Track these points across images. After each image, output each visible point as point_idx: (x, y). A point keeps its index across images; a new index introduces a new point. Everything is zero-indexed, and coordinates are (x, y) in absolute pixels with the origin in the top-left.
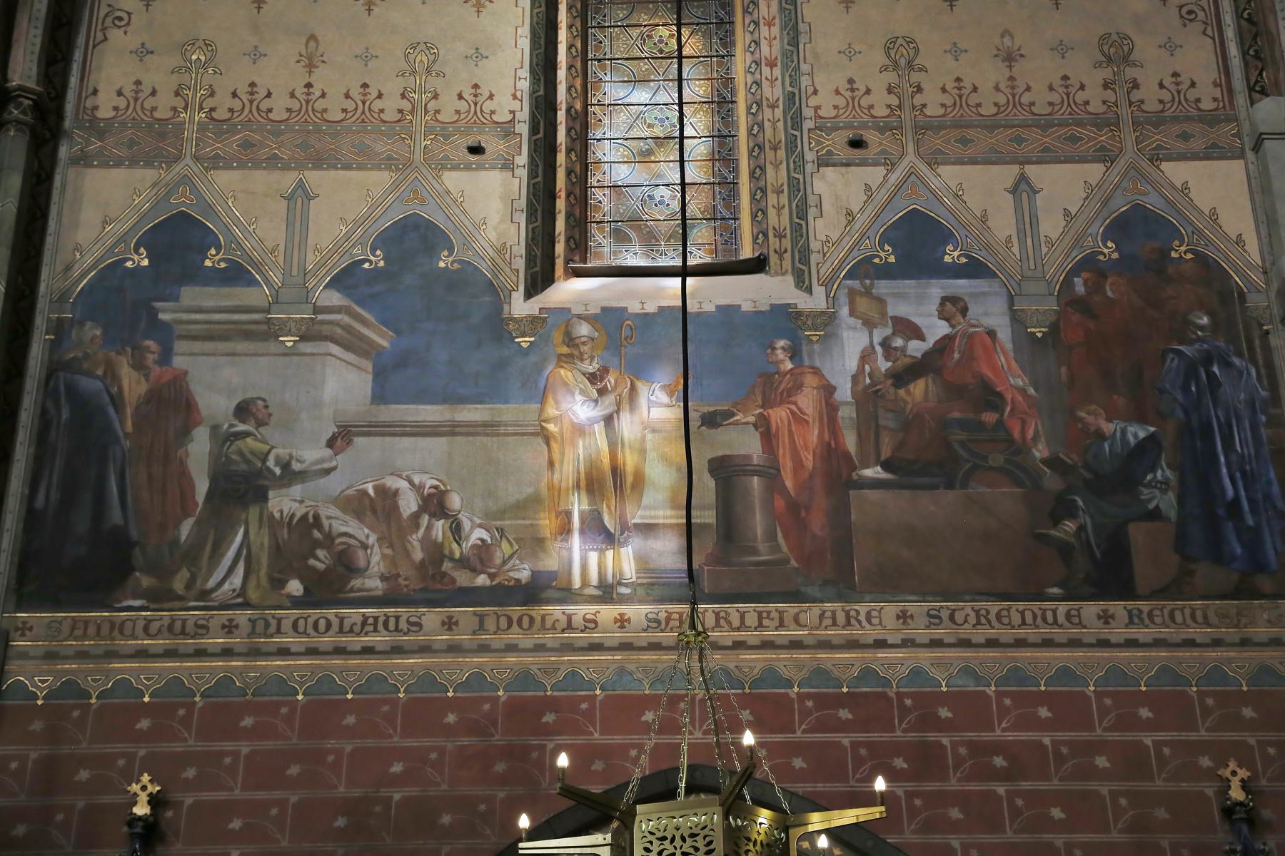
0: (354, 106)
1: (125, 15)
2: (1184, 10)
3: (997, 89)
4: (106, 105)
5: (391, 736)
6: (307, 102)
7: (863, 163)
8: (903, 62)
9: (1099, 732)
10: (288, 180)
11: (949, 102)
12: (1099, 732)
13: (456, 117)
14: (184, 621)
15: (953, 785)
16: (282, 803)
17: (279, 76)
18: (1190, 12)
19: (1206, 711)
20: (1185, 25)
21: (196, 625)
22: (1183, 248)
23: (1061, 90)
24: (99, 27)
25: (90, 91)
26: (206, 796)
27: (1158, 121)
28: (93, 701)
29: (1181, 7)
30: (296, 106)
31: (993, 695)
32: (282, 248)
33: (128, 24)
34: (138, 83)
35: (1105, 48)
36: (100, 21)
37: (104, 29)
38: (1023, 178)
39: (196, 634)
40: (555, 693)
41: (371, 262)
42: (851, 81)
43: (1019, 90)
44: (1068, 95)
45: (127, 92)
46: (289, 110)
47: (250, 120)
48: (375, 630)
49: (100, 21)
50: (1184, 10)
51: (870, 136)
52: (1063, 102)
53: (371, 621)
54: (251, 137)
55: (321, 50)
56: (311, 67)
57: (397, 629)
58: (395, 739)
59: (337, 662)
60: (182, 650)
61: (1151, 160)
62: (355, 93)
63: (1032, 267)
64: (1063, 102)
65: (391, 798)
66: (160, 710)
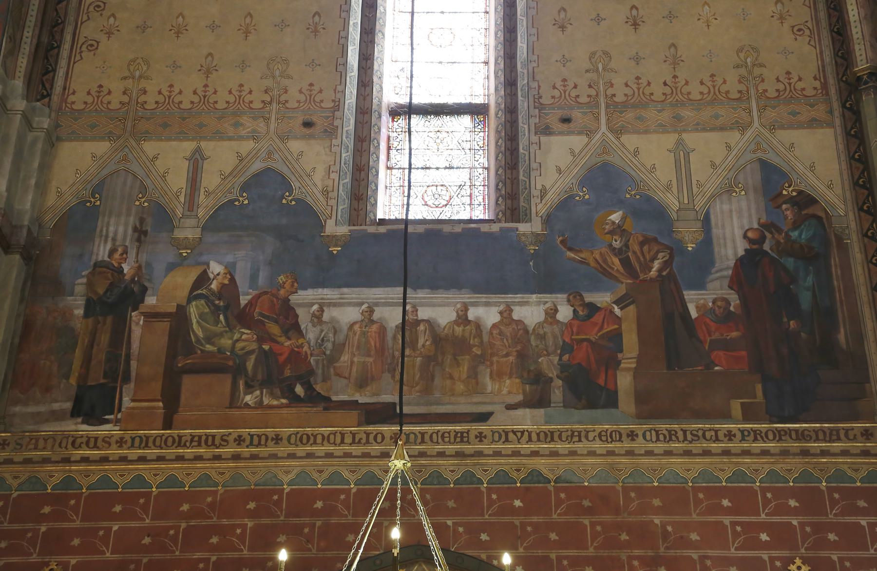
0: (304, 98)
1: (94, 43)
2: (796, 29)
3: (195, 93)
4: (78, 99)
5: (74, 521)
6: (98, 97)
7: (569, 133)
8: (277, 73)
9: (763, 516)
10: (189, 147)
11: (706, 91)
12: (763, 516)
13: (226, 105)
14: (214, 437)
15: (733, 552)
16: (207, 561)
17: (189, 83)
18: (799, 30)
19: (491, 502)
20: (796, 39)
21: (103, 440)
22: (790, 189)
23: (307, 93)
24: (78, 51)
25: (71, 91)
26: (157, 556)
27: (625, 106)
28: (154, 489)
29: (793, 27)
30: (781, 87)
31: (824, 489)
32: (674, 182)
33: (97, 48)
34: (311, 85)
35: (132, 68)
36: (79, 46)
37: (81, 52)
38: (680, 143)
39: (220, 444)
40: (729, 485)
41: (91, 202)
42: (564, 80)
43: (314, 92)
44: (790, 84)
45: (93, 93)
46: (157, 102)
47: (791, 97)
48: (580, 441)
49: (79, 46)
50: (796, 29)
51: (576, 114)
52: (561, 96)
53: (196, 439)
54: (174, 120)
55: (679, 53)
56: (208, 73)
57: (213, 444)
58: (6, 524)
59: (646, 460)
60: (832, 451)
61: (770, 130)
62: (559, 84)
63: (686, 202)
64: (561, 96)
65: (69, 562)
66: (58, 499)
